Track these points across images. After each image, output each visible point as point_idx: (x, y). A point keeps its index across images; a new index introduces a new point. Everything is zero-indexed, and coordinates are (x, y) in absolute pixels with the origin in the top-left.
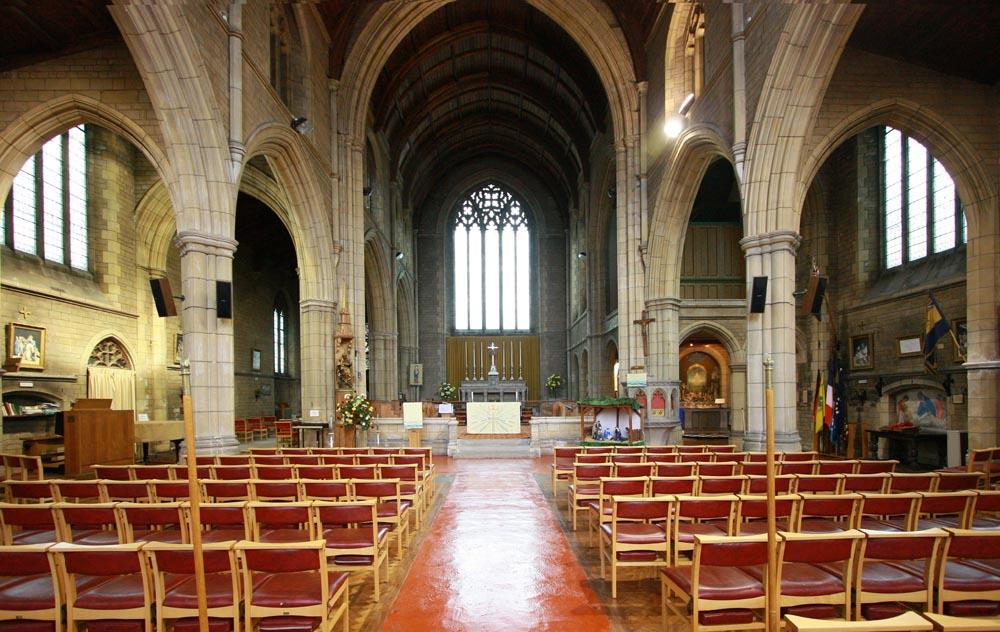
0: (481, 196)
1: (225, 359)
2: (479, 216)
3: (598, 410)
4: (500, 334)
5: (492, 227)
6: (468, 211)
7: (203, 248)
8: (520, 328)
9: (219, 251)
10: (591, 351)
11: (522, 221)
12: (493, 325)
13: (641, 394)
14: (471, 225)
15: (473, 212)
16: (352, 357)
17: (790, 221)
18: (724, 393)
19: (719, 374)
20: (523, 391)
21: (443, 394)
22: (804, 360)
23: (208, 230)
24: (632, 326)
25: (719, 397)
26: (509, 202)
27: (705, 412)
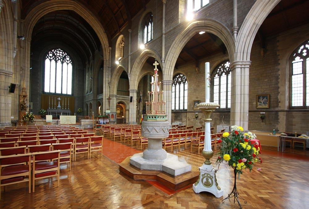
0: (56, 51)
1: (10, 103)
2: (55, 57)
3: (99, 118)
4: (61, 95)
5: (59, 63)
6: (51, 55)
7: (5, 74)
8: (68, 94)
9: (9, 75)
10: (93, 103)
11: (70, 62)
12: (59, 92)
13: (109, 114)
14: (52, 60)
15: (53, 56)
16: (25, 102)
17: (136, 88)
18: (124, 115)
19: (123, 110)
20: (70, 112)
21: (41, 113)
22: (139, 109)
23: (7, 70)
24: (106, 100)
25: (123, 116)
26: (66, 56)
27: (120, 119)
